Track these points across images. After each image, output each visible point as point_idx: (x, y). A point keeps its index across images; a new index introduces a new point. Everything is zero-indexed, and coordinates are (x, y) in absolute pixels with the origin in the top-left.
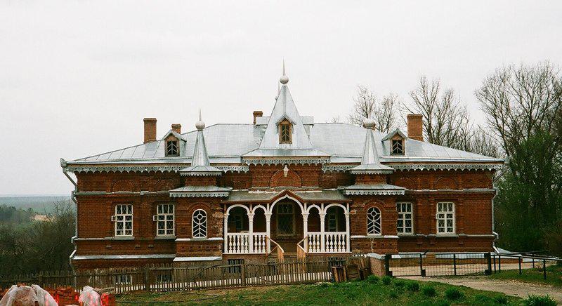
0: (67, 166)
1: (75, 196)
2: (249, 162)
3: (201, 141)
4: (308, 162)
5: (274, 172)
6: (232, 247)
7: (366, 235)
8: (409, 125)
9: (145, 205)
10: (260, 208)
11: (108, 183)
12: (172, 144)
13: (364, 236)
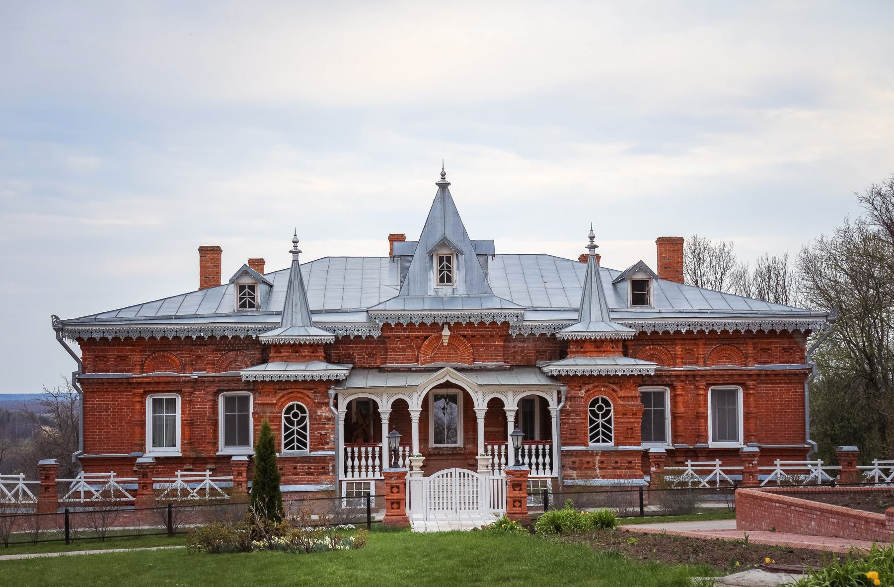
0: (62, 328)
1: (79, 380)
2: (381, 319)
3: (296, 283)
4: (496, 319)
5: (426, 338)
6: (353, 467)
7: (586, 445)
8: (660, 255)
9: (201, 396)
10: (495, 398)
11: (136, 358)
12: (247, 290)
13: (583, 448)
